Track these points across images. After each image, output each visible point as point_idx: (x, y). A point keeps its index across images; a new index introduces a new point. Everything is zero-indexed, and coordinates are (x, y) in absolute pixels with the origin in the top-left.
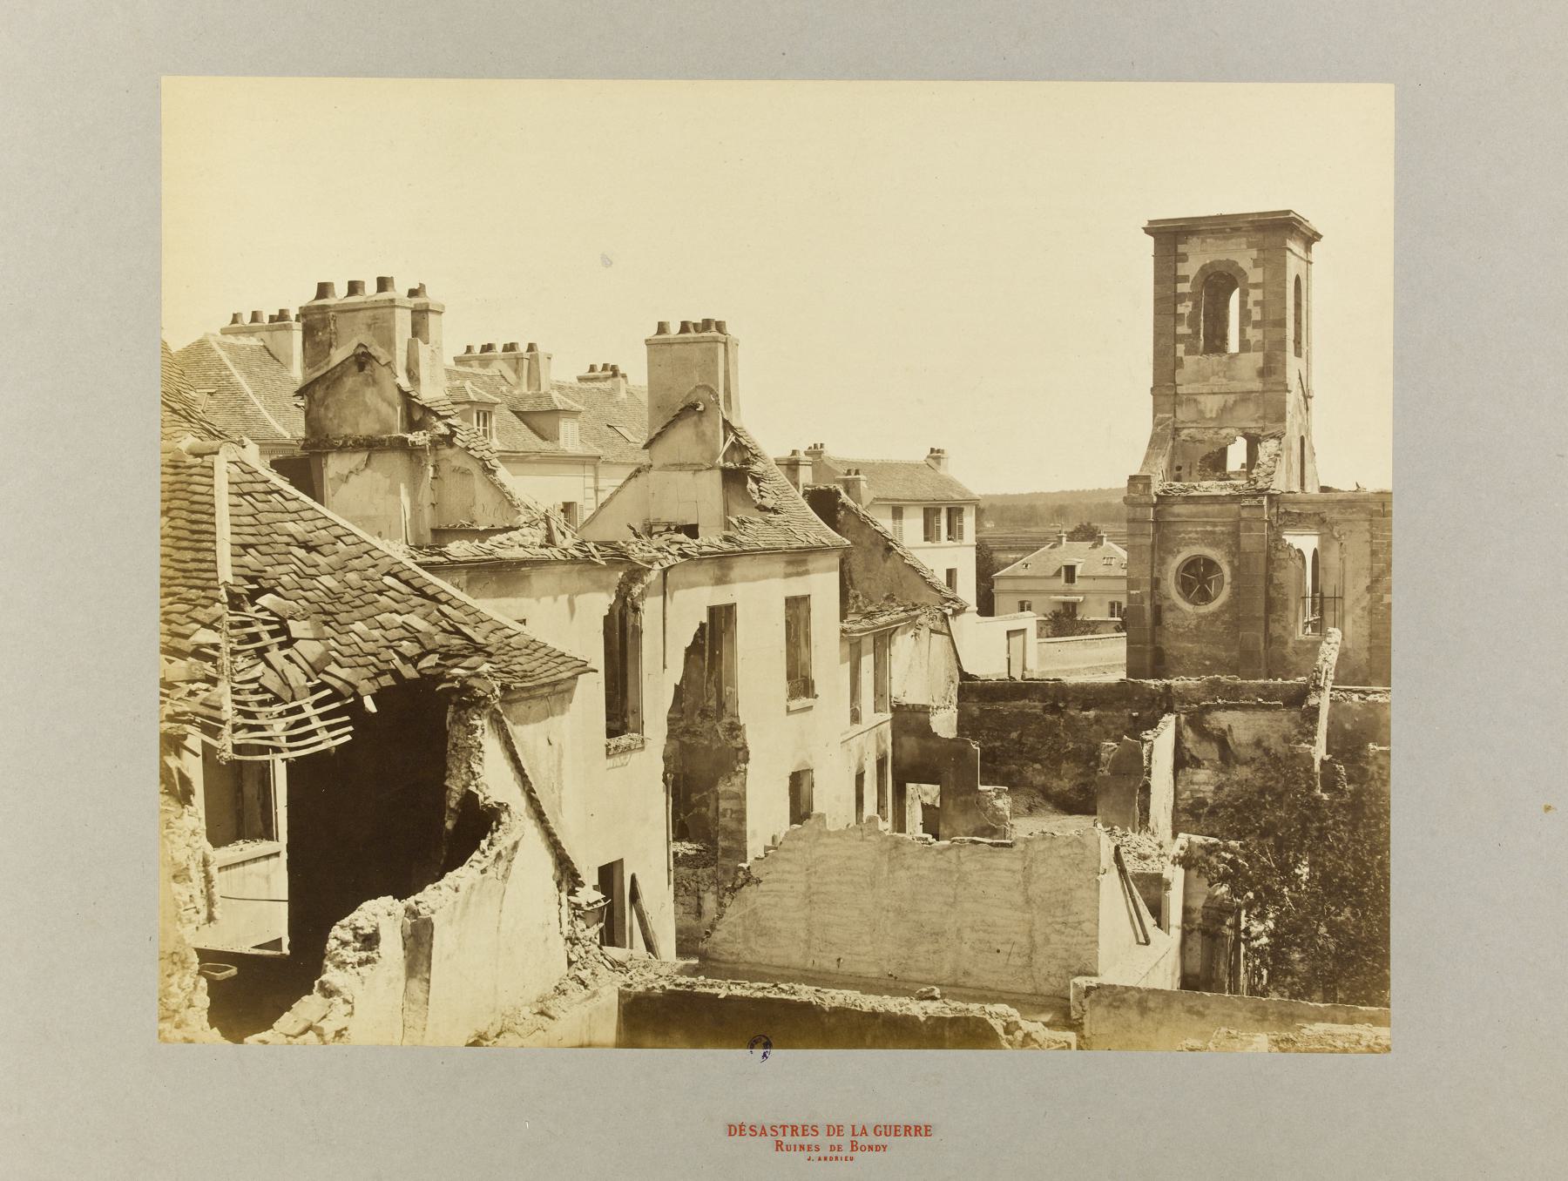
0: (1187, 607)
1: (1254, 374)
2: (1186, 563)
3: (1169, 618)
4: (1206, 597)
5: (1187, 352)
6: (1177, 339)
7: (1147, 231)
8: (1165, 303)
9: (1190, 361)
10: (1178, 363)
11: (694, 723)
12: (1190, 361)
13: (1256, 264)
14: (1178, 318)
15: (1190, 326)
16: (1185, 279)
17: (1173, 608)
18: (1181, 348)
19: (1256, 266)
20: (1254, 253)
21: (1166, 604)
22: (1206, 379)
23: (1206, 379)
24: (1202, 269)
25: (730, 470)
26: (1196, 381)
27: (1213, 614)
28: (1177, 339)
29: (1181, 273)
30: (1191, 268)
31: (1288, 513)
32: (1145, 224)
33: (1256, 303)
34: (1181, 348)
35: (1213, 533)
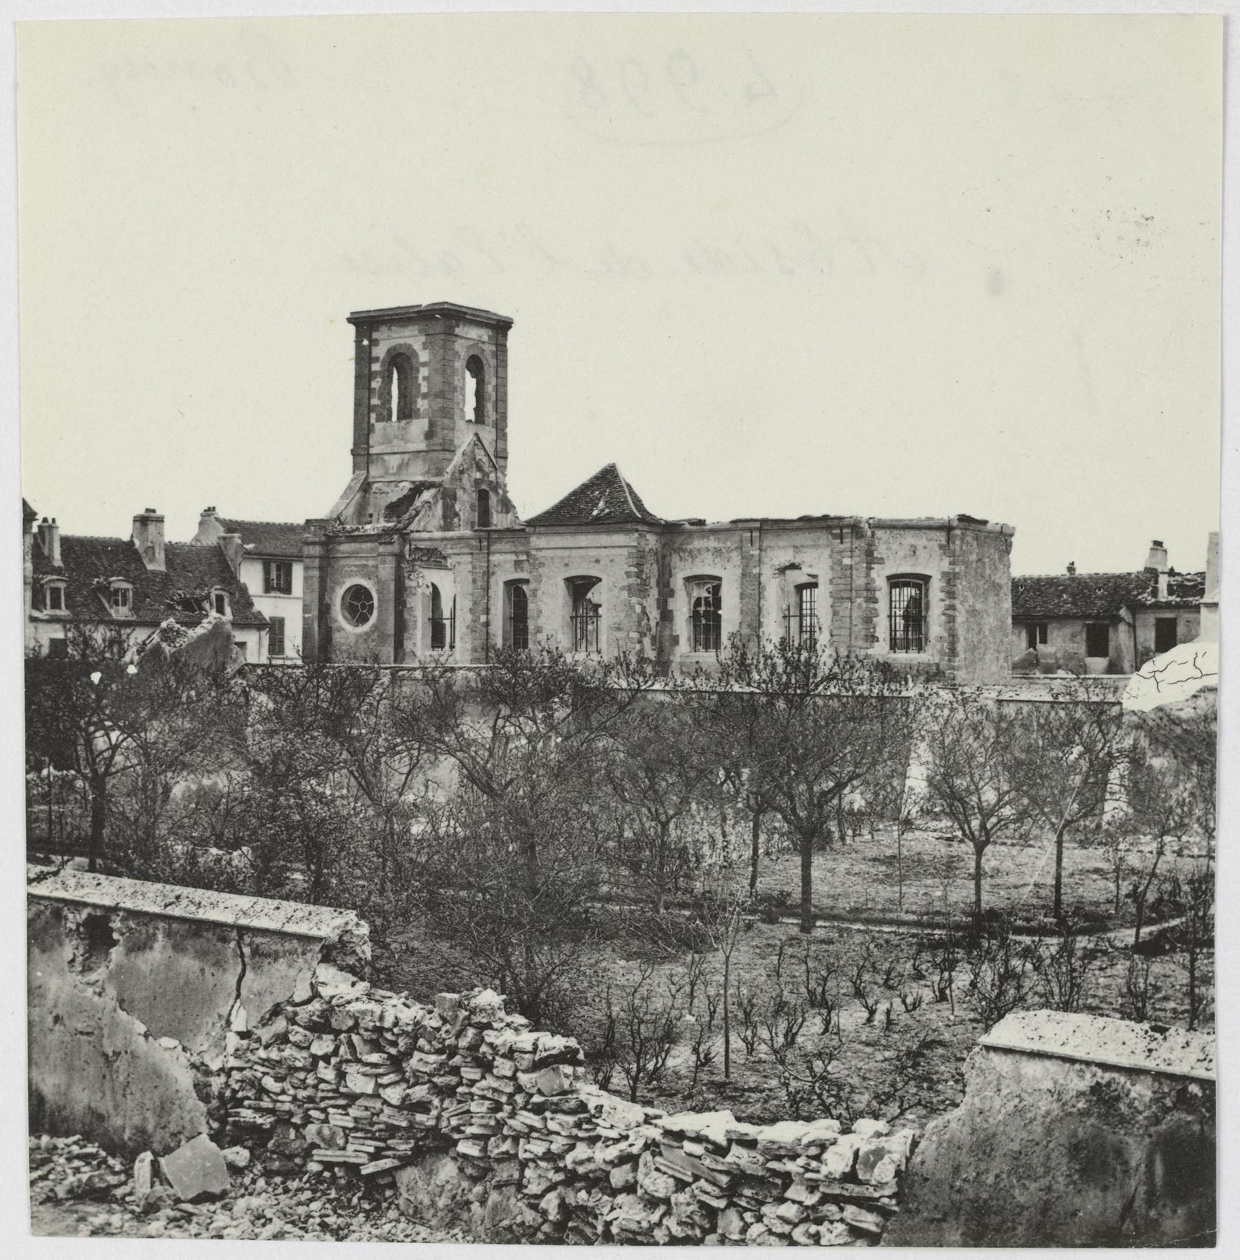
0: (348, 628)
1: (422, 437)
2: (29, 557)
3: (337, 637)
4: (363, 619)
5: (378, 420)
6: (370, 409)
7: (349, 320)
8: (363, 379)
9: (379, 426)
10: (370, 429)
11: (358, 709)
12: (379, 426)
13: (425, 346)
14: (370, 390)
15: (380, 398)
16: (377, 359)
17: (340, 629)
18: (373, 416)
19: (425, 348)
20: (423, 338)
21: (334, 626)
22: (390, 442)
23: (390, 442)
24: (389, 351)
25: (1175, 629)
26: (383, 443)
27: (366, 633)
28: (370, 409)
29: (374, 354)
30: (380, 351)
31: (417, 549)
32: (348, 315)
33: (425, 379)
34: (373, 416)
35: (365, 566)
